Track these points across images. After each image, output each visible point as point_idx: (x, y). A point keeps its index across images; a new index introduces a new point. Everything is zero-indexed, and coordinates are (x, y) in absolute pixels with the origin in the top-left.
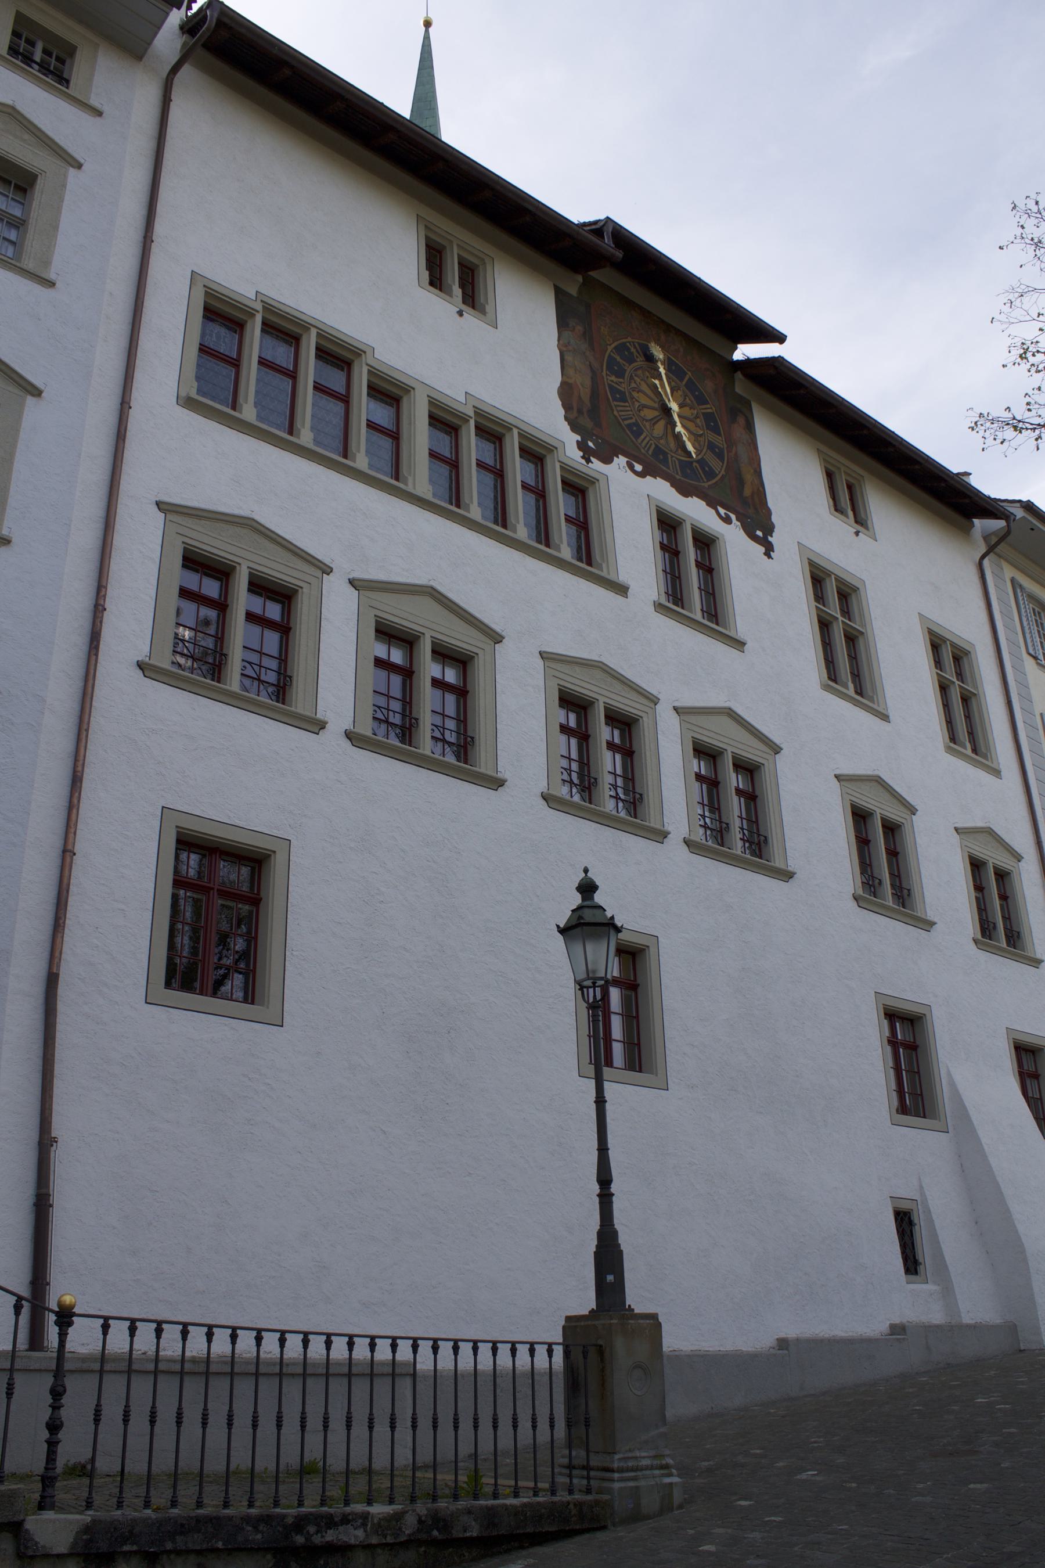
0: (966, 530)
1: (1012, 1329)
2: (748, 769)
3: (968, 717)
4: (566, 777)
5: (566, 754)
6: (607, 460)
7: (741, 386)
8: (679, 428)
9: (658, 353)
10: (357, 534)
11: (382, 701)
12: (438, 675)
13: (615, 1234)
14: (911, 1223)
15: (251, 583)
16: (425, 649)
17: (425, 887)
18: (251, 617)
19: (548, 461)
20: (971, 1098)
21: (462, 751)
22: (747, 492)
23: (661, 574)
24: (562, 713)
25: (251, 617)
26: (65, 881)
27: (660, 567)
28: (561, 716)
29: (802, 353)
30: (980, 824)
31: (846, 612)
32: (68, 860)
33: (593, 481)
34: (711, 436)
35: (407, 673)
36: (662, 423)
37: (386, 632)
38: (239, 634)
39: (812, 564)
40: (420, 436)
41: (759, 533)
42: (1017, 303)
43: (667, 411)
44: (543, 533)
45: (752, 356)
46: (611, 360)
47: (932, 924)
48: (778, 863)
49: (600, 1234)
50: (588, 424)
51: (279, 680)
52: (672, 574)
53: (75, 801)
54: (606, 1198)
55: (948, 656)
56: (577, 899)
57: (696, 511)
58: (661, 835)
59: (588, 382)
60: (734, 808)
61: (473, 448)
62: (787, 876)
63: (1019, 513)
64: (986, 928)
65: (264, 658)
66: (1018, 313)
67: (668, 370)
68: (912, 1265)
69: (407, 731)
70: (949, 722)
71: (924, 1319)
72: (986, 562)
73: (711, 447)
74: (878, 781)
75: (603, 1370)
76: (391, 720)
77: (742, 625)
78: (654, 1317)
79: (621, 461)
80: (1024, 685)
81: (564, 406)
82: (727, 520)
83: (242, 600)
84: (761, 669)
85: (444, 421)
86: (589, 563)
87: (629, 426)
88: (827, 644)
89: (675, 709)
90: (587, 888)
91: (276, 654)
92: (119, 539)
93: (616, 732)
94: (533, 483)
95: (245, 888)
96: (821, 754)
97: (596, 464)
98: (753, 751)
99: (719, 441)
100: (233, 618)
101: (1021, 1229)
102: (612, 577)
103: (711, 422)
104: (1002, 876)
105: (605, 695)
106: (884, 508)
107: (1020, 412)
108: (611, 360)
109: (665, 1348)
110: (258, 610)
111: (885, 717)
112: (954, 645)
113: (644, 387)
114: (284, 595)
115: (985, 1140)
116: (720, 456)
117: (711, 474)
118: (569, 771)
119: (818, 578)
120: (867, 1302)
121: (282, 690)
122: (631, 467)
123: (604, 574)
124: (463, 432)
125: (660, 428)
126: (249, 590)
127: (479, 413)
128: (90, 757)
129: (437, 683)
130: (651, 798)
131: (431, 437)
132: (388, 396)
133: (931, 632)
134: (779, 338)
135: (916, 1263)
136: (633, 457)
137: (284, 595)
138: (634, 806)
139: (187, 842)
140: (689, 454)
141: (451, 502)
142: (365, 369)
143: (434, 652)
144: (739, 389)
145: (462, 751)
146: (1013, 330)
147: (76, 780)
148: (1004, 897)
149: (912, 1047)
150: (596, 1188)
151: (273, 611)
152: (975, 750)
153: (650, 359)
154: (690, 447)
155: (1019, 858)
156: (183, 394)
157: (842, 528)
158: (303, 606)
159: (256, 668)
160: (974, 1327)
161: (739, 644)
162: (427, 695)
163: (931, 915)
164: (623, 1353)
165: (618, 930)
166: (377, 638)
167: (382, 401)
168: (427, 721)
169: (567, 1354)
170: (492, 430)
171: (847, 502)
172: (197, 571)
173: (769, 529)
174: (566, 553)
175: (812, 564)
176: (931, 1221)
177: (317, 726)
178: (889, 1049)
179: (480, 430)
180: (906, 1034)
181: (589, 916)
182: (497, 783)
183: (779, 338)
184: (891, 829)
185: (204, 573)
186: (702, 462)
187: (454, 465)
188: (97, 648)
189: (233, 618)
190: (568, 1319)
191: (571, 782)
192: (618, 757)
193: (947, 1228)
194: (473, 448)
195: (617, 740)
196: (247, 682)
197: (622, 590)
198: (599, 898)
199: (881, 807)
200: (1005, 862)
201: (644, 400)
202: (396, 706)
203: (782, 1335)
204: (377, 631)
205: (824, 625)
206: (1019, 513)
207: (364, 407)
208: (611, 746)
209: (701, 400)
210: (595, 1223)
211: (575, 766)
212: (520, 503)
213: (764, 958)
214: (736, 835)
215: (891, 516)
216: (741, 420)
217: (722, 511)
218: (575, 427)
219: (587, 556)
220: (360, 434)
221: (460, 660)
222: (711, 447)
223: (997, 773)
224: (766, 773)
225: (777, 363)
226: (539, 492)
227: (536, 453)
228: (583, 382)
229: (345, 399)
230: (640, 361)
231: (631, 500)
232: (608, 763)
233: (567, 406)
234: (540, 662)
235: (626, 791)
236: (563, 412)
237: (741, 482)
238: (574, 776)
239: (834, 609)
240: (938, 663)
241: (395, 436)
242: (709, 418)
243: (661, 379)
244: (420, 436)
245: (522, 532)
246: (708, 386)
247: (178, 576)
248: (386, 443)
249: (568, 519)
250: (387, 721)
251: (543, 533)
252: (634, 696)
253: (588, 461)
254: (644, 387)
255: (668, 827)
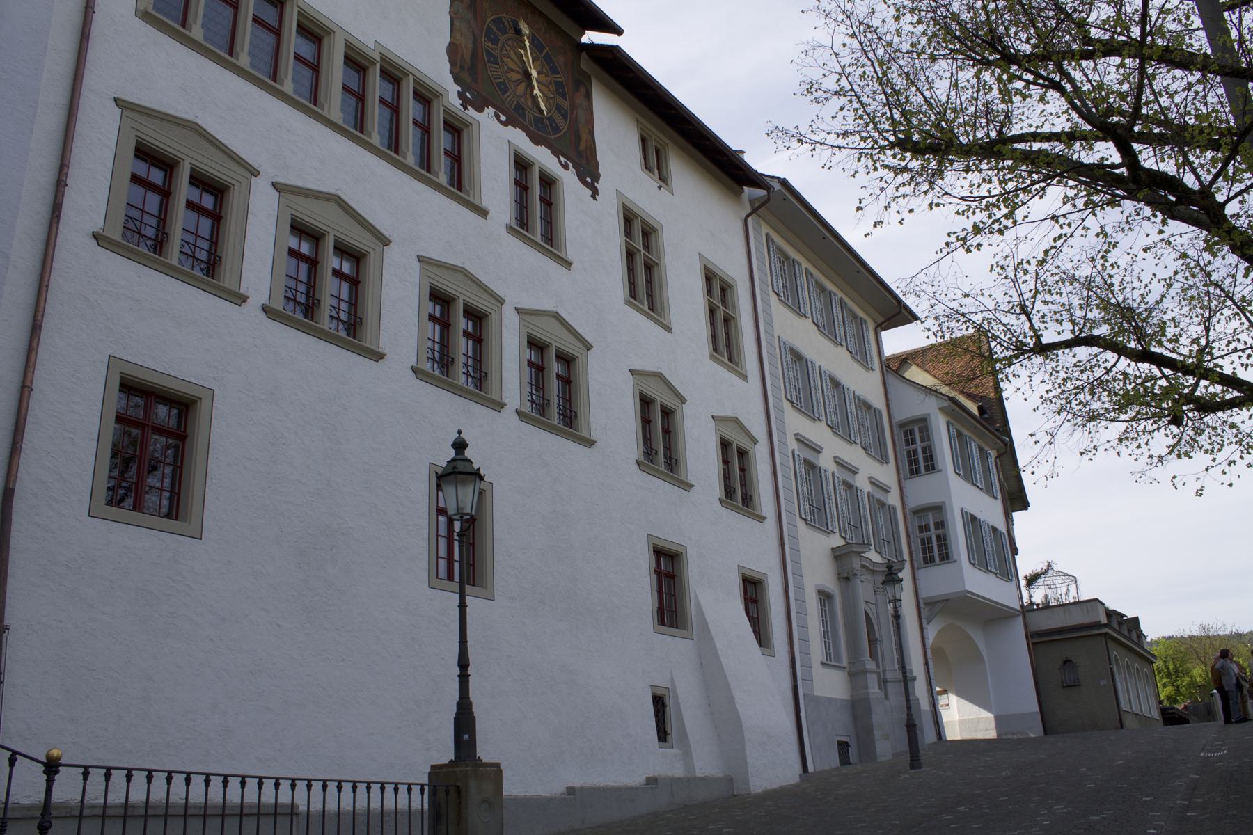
0: (738, 194)
1: (729, 780)
2: (566, 360)
3: (727, 334)
4: (430, 355)
5: (336, 294)
6: (480, 109)
7: (585, 63)
8: (536, 91)
9: (525, 29)
10: (282, 147)
11: (292, 284)
12: (337, 267)
13: (470, 704)
14: (664, 705)
15: (191, 177)
16: (329, 245)
17: (332, 438)
18: (190, 205)
19: (435, 105)
20: (710, 617)
21: (353, 329)
22: (582, 147)
23: (513, 204)
24: (431, 305)
25: (190, 205)
26: (23, 411)
27: (513, 198)
28: (429, 307)
29: (635, 45)
30: (730, 414)
31: (647, 247)
32: (26, 393)
33: (468, 125)
34: (560, 100)
35: (313, 263)
36: (523, 86)
37: (299, 228)
38: (180, 218)
39: (625, 207)
40: (336, 73)
41: (589, 180)
42: (810, 53)
43: (528, 76)
44: (426, 161)
45: (596, 42)
46: (489, 30)
47: (691, 486)
48: (584, 433)
49: (459, 704)
50: (468, 79)
51: (157, 235)
52: (521, 204)
53: (35, 345)
54: (464, 678)
55: (717, 288)
56: (452, 453)
57: (543, 157)
58: (499, 406)
59: (470, 45)
60: (554, 387)
61: (377, 87)
62: (590, 443)
63: (777, 187)
64: (729, 492)
65: (145, 216)
66: (810, 60)
67: (532, 43)
68: (663, 735)
69: (310, 308)
70: (714, 337)
71: (670, 774)
72: (750, 220)
73: (559, 108)
74: (660, 376)
75: (460, 803)
76: (298, 299)
77: (570, 250)
78: (497, 765)
79: (490, 111)
80: (768, 314)
81: (450, 62)
82: (566, 167)
83: (184, 191)
84: (581, 287)
85: (356, 62)
86: (459, 189)
87: (498, 84)
88: (631, 270)
89: (517, 309)
90: (460, 446)
91: (156, 213)
92: (81, 127)
93: (470, 323)
94: (389, 100)
95: (173, 422)
96: (619, 349)
97: (471, 112)
98: (571, 347)
99: (565, 105)
100: (175, 203)
101: (740, 710)
102: (477, 202)
103: (560, 89)
104: (742, 453)
105: (464, 295)
106: (680, 170)
107: (804, 130)
108: (489, 30)
109: (992, 734)
110: (195, 199)
111: (668, 329)
112: (721, 280)
113: (512, 54)
114: (218, 190)
115: (719, 646)
116: (564, 116)
117: (556, 130)
118: (433, 351)
119: (629, 218)
120: (630, 761)
121: (212, 266)
122: (498, 118)
123: (471, 199)
124: (370, 72)
125: (521, 88)
126: (190, 183)
127: (384, 59)
128: (49, 309)
129: (337, 273)
130: (493, 377)
131: (345, 73)
132: (310, 34)
133: (706, 268)
134: (618, 31)
135: (666, 733)
136: (499, 109)
137: (218, 190)
138: (480, 382)
139: (129, 387)
140: (542, 112)
141: (356, 128)
142: (296, 10)
143: (335, 248)
144: (583, 66)
145: (353, 329)
146: (804, 71)
147: (36, 328)
148: (742, 470)
149: (671, 576)
150: (457, 671)
151: (208, 201)
152: (730, 359)
153: (518, 32)
154: (543, 107)
155: (755, 441)
156: (141, 7)
157: (649, 182)
158: (234, 201)
159: (138, 224)
160: (704, 779)
161: (567, 264)
162: (328, 280)
163: (691, 480)
164: (475, 793)
165: (482, 478)
166: (292, 232)
167: (307, 38)
168: (327, 303)
169: (433, 793)
170: (393, 74)
171: (654, 163)
172: (146, 161)
173: (596, 177)
174: (443, 179)
175: (625, 207)
176: (678, 704)
177: (240, 299)
178: (654, 576)
179: (384, 72)
180: (668, 565)
181: (461, 466)
182: (378, 356)
183: (618, 31)
184: (667, 413)
185: (152, 165)
186: (550, 119)
187: (361, 98)
188: (58, 217)
189: (175, 203)
190: (433, 767)
191: (338, 319)
192: (470, 342)
193: (690, 711)
194: (377, 87)
195: (470, 330)
196: (183, 258)
197: (483, 213)
198: (468, 453)
199: (661, 397)
200: (745, 443)
201: (513, 66)
202: (302, 288)
203: (571, 785)
204: (292, 227)
205: (630, 255)
206: (777, 187)
207: (293, 43)
208: (466, 333)
209: (554, 71)
210: (456, 696)
211: (437, 347)
212: (410, 136)
213: (572, 506)
214: (554, 410)
215: (687, 182)
216: (582, 90)
217: (563, 160)
218: (457, 80)
219: (459, 183)
220: (288, 65)
221: (356, 257)
222: (559, 108)
223: (744, 377)
224: (580, 363)
225: (614, 51)
226: (425, 128)
227: (426, 96)
228: (466, 45)
229: (277, 32)
230: (511, 34)
231: (495, 142)
232: (462, 346)
233: (453, 63)
234: (416, 264)
235: (474, 370)
236: (449, 66)
237: (578, 138)
238: (437, 355)
239: (638, 244)
240: (709, 292)
241: (315, 69)
242: (559, 85)
243: (525, 50)
244: (336, 73)
245: (411, 159)
246: (560, 60)
247: (131, 164)
248: (307, 73)
249: (447, 153)
250: (295, 300)
251: (426, 161)
252: (486, 296)
253: (466, 108)
254: (512, 54)
255: (505, 400)
